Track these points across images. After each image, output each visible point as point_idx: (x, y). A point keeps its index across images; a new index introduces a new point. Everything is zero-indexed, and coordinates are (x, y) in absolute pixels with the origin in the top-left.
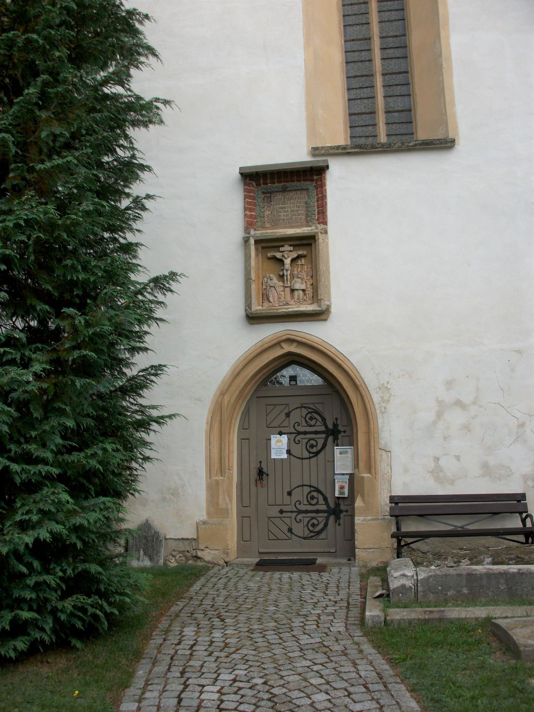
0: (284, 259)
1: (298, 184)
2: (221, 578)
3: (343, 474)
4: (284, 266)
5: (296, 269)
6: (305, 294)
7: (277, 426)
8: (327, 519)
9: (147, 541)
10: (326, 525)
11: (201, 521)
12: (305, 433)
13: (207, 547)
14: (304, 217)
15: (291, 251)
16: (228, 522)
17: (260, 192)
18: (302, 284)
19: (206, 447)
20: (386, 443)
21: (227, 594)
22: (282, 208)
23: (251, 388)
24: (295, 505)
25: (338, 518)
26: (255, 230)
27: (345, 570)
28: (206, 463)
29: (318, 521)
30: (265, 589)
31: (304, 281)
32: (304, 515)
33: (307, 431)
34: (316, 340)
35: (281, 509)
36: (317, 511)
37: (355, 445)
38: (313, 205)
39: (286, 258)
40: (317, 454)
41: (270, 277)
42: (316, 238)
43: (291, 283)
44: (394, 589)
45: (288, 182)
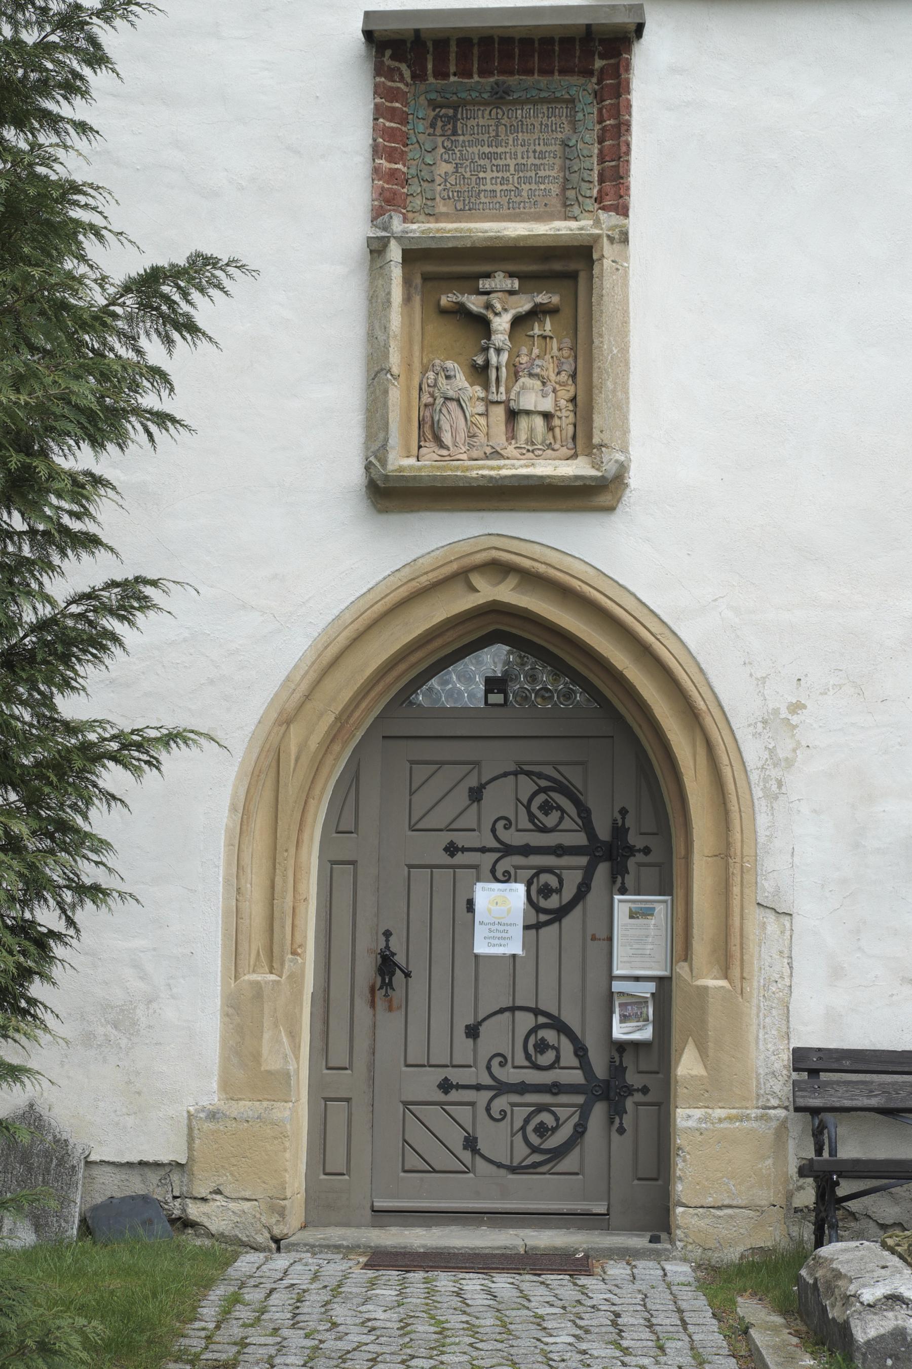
0: (491, 316)
1: (543, 81)
2: (272, 1291)
3: (637, 979)
4: (489, 338)
5: (524, 350)
6: (551, 429)
7: (442, 827)
8: (585, 1112)
9: (30, 1169)
10: (580, 1131)
11: (203, 1109)
12: (526, 850)
13: (218, 1192)
14: (555, 189)
15: (511, 293)
16: (287, 1113)
17: (422, 100)
18: (544, 396)
19: (227, 881)
20: (778, 890)
21: (309, 1343)
22: (485, 156)
23: (369, 709)
24: (489, 1068)
25: (616, 1111)
26: (405, 220)
27: (647, 1269)
28: (226, 930)
29: (557, 1119)
30: (423, 1328)
31: (549, 388)
32: (516, 1098)
33: (532, 844)
34: (578, 568)
35: (446, 1079)
36: (555, 1089)
37: (679, 891)
38: (585, 153)
39: (497, 314)
40: (559, 914)
41: (444, 369)
42: (595, 257)
43: (508, 391)
44: (868, 1343)
45: (511, 73)
